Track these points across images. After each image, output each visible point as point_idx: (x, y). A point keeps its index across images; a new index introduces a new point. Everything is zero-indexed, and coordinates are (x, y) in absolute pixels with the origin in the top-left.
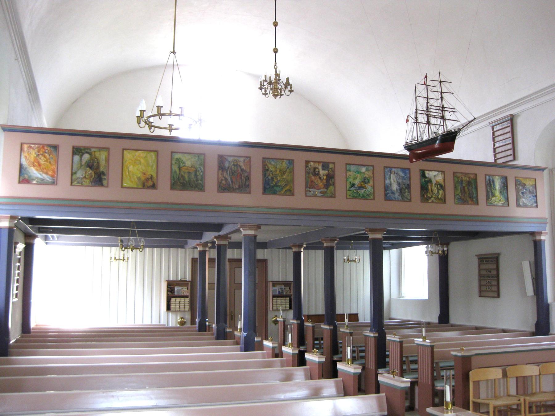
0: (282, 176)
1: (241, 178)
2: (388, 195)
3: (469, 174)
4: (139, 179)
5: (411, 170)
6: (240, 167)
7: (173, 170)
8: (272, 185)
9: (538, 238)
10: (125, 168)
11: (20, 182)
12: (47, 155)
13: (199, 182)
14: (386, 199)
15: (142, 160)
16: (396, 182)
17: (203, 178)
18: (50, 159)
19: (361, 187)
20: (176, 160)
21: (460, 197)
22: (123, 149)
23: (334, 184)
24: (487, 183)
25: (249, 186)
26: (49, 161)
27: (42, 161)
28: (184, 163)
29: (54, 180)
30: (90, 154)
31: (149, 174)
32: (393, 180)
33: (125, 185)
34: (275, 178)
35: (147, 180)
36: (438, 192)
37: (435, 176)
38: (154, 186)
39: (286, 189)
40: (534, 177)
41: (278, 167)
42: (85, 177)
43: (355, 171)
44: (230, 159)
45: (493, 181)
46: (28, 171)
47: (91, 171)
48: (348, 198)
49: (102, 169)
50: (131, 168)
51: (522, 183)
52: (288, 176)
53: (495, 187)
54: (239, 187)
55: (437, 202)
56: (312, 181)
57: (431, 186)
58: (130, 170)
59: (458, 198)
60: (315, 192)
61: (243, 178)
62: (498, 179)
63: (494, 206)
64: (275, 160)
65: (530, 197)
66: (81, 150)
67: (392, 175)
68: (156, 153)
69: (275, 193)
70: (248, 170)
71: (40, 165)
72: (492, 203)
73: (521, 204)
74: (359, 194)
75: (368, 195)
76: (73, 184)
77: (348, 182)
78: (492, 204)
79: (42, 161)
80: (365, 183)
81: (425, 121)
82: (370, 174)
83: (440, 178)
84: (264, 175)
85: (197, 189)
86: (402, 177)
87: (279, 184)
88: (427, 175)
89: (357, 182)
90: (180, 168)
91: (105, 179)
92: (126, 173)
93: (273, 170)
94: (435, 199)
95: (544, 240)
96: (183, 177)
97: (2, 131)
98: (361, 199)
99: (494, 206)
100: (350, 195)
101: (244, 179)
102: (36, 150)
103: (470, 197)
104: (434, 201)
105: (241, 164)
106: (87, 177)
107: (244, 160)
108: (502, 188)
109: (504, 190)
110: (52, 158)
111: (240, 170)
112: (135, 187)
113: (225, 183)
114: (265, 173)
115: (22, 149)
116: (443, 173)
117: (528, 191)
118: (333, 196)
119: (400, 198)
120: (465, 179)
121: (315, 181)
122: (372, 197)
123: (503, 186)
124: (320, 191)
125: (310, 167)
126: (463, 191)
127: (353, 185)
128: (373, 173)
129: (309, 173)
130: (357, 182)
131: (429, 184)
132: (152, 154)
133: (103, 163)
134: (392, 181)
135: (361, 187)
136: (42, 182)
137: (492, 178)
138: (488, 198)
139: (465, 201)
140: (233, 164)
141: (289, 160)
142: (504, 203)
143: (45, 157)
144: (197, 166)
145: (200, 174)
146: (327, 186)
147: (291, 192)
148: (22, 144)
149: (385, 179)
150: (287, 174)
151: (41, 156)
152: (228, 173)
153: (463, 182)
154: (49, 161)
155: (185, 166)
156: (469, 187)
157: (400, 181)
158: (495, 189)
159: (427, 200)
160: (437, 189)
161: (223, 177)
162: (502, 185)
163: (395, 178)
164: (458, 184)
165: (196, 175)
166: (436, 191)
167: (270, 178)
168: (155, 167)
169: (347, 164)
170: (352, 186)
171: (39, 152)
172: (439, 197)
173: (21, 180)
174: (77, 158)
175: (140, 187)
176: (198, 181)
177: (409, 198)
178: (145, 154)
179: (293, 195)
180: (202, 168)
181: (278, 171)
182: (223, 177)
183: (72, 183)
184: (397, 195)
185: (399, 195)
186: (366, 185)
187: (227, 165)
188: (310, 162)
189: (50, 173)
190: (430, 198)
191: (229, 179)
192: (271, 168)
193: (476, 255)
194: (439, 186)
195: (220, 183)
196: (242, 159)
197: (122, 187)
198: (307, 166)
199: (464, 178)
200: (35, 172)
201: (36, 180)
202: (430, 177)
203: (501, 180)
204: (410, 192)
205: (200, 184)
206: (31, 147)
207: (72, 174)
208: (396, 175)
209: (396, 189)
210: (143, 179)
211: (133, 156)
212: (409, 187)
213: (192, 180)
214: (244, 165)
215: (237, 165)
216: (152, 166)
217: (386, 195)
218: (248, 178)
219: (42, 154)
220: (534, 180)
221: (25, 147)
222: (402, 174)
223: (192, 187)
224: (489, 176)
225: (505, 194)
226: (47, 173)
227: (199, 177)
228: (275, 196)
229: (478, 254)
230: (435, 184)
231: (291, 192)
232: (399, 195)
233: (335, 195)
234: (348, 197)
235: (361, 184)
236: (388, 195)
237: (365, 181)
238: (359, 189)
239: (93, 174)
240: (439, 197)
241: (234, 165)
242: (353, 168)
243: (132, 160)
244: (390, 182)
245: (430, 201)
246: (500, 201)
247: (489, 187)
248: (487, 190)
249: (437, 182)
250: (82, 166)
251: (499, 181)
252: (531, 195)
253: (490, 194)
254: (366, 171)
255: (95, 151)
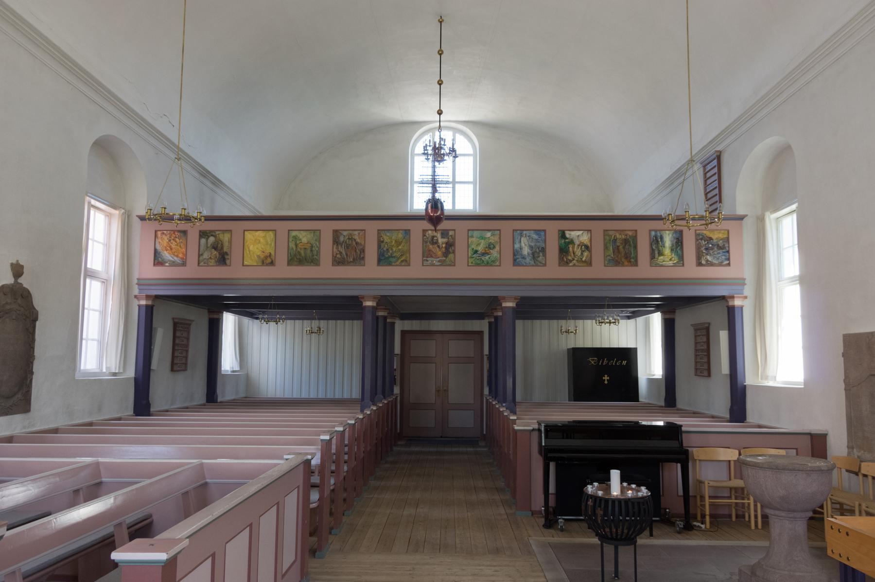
0: (398, 247)
1: (356, 251)
2: (518, 260)
3: (626, 230)
4: (259, 256)
5: (547, 231)
6: (355, 240)
7: (290, 246)
8: (387, 256)
9: (731, 303)
10: (246, 247)
11: (154, 265)
12: (177, 240)
13: (315, 257)
14: (514, 265)
15: (262, 240)
16: (528, 245)
17: (318, 252)
18: (180, 243)
19: (484, 254)
20: (293, 238)
21: (612, 258)
22: (244, 231)
23: (454, 252)
24: (652, 240)
25: (363, 258)
26: (179, 245)
27: (173, 245)
28: (300, 240)
29: (184, 261)
30: (215, 236)
31: (267, 252)
32: (524, 243)
33: (246, 263)
34: (390, 249)
35: (266, 257)
36: (582, 254)
37: (578, 236)
38: (272, 263)
39: (402, 259)
40: (727, 228)
41: (393, 238)
42: (211, 258)
43: (479, 236)
44: (345, 233)
45: (662, 238)
46: (161, 255)
47: (216, 252)
48: (470, 266)
49: (225, 249)
50: (251, 247)
51: (707, 237)
52: (404, 246)
53: (664, 245)
54: (354, 259)
55: (580, 265)
56: (430, 251)
57: (573, 248)
58: (250, 249)
59: (610, 260)
60: (432, 261)
61: (357, 251)
62: (669, 234)
63: (662, 266)
64: (390, 231)
65: (719, 253)
66: (207, 233)
67: (522, 239)
68: (274, 232)
69: (390, 264)
70: (363, 243)
71: (171, 249)
72: (659, 263)
73: (703, 262)
74: (483, 261)
75: (493, 261)
76: (200, 265)
77: (470, 249)
78: (658, 264)
79: (173, 245)
80: (490, 249)
81: (441, 188)
82: (497, 238)
83: (585, 238)
84: (379, 247)
85: (312, 264)
86: (535, 239)
87: (394, 255)
88: (568, 236)
89: (480, 249)
90: (296, 245)
91: (228, 259)
92: (247, 252)
93: (389, 241)
94: (578, 262)
95: (742, 308)
96: (300, 253)
97: (139, 220)
98: (485, 266)
99: (662, 266)
100: (472, 263)
101: (359, 252)
102: (168, 236)
103: (626, 258)
104: (577, 264)
105: (356, 237)
106: (212, 257)
107: (359, 234)
108: (675, 245)
109: (677, 248)
110: (182, 242)
111: (354, 243)
112: (255, 264)
113: (340, 257)
114: (380, 245)
115: (156, 236)
116: (589, 232)
117: (716, 246)
118: (453, 264)
119: (532, 263)
120: (620, 237)
121: (433, 250)
122: (498, 263)
123: (676, 242)
124: (438, 259)
125: (427, 236)
126: (616, 251)
127: (476, 252)
128: (500, 238)
129: (426, 242)
130: (480, 249)
131: (571, 246)
132: (271, 233)
133: (226, 244)
134: (523, 245)
135: (484, 254)
136: (173, 264)
137: (660, 233)
138: (653, 257)
139: (620, 263)
140: (347, 237)
141: (405, 230)
142: (677, 262)
143: (176, 242)
144: (313, 242)
145: (315, 249)
146: (446, 254)
147: (407, 263)
148: (156, 232)
149: (514, 243)
150: (403, 244)
151: (172, 241)
152: (343, 246)
153: (617, 240)
154: (179, 245)
155: (301, 242)
156: (625, 246)
157: (533, 244)
158: (664, 247)
159: (567, 263)
160: (580, 251)
161: (338, 251)
162: (675, 241)
163: (526, 241)
164: (610, 243)
165: (312, 251)
166: (580, 253)
167: (385, 249)
168: (273, 245)
169: (469, 230)
170: (474, 253)
171: (170, 237)
172: (584, 259)
173: (155, 264)
174: (203, 241)
175: (260, 264)
176: (314, 256)
177: (544, 262)
178: (265, 233)
179: (409, 265)
180: (318, 244)
181: (394, 242)
182: (338, 251)
183: (199, 264)
184: (528, 260)
185: (530, 260)
186: (491, 251)
187: (342, 239)
188: (427, 230)
189: (181, 255)
190: (571, 261)
191: (344, 253)
192: (386, 239)
193: (692, 325)
194: (583, 247)
195: (335, 257)
196: (356, 233)
197: (243, 265)
198: (424, 235)
199: (618, 236)
200: (167, 255)
201: (169, 262)
202: (571, 237)
203: (673, 235)
204: (545, 255)
205: (316, 259)
206: (163, 233)
207: (200, 255)
208: (528, 238)
209: (528, 253)
210: (262, 257)
211: (253, 236)
212: (543, 250)
213: (308, 255)
214: (359, 238)
215: (351, 239)
216: (271, 245)
217: (515, 260)
218: (363, 251)
219: (173, 239)
220: (726, 232)
221: (159, 233)
222: (535, 236)
223: (308, 262)
224: (656, 231)
225: (679, 251)
226: (177, 256)
227: (315, 253)
228: (391, 267)
229: (693, 323)
230: (579, 245)
231: (407, 263)
232: (530, 260)
233: (455, 263)
234: (470, 264)
235: (485, 250)
236: (517, 259)
237: (491, 246)
238: (483, 256)
239: (218, 254)
240: (584, 259)
241: (349, 239)
242: (476, 234)
243: (252, 240)
244: (520, 246)
245: (570, 265)
246: (670, 260)
247: (655, 244)
248: (652, 247)
249: (581, 243)
250: (208, 248)
251: (671, 235)
252: (721, 251)
253: (656, 252)
254: (491, 236)
255: (219, 234)
